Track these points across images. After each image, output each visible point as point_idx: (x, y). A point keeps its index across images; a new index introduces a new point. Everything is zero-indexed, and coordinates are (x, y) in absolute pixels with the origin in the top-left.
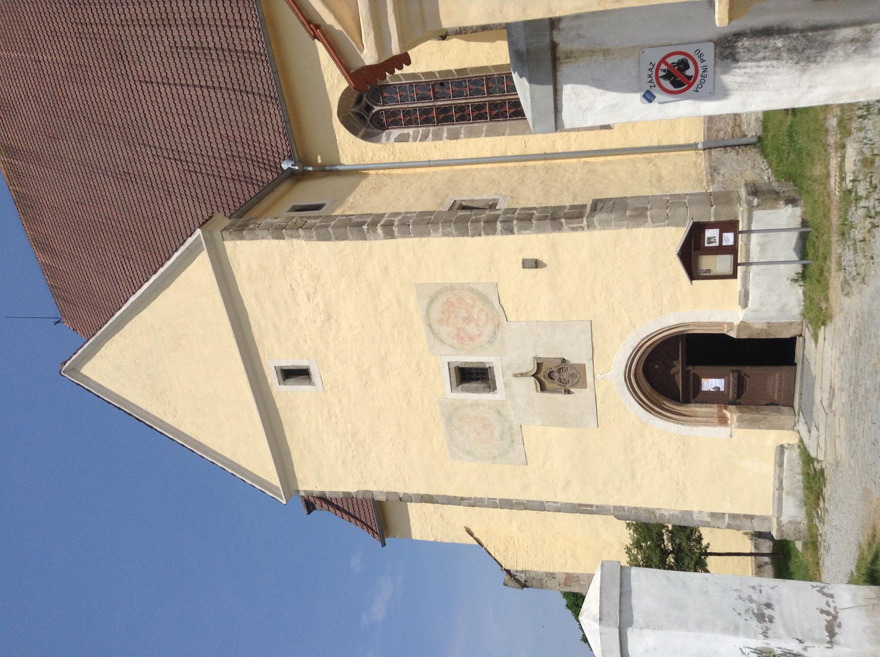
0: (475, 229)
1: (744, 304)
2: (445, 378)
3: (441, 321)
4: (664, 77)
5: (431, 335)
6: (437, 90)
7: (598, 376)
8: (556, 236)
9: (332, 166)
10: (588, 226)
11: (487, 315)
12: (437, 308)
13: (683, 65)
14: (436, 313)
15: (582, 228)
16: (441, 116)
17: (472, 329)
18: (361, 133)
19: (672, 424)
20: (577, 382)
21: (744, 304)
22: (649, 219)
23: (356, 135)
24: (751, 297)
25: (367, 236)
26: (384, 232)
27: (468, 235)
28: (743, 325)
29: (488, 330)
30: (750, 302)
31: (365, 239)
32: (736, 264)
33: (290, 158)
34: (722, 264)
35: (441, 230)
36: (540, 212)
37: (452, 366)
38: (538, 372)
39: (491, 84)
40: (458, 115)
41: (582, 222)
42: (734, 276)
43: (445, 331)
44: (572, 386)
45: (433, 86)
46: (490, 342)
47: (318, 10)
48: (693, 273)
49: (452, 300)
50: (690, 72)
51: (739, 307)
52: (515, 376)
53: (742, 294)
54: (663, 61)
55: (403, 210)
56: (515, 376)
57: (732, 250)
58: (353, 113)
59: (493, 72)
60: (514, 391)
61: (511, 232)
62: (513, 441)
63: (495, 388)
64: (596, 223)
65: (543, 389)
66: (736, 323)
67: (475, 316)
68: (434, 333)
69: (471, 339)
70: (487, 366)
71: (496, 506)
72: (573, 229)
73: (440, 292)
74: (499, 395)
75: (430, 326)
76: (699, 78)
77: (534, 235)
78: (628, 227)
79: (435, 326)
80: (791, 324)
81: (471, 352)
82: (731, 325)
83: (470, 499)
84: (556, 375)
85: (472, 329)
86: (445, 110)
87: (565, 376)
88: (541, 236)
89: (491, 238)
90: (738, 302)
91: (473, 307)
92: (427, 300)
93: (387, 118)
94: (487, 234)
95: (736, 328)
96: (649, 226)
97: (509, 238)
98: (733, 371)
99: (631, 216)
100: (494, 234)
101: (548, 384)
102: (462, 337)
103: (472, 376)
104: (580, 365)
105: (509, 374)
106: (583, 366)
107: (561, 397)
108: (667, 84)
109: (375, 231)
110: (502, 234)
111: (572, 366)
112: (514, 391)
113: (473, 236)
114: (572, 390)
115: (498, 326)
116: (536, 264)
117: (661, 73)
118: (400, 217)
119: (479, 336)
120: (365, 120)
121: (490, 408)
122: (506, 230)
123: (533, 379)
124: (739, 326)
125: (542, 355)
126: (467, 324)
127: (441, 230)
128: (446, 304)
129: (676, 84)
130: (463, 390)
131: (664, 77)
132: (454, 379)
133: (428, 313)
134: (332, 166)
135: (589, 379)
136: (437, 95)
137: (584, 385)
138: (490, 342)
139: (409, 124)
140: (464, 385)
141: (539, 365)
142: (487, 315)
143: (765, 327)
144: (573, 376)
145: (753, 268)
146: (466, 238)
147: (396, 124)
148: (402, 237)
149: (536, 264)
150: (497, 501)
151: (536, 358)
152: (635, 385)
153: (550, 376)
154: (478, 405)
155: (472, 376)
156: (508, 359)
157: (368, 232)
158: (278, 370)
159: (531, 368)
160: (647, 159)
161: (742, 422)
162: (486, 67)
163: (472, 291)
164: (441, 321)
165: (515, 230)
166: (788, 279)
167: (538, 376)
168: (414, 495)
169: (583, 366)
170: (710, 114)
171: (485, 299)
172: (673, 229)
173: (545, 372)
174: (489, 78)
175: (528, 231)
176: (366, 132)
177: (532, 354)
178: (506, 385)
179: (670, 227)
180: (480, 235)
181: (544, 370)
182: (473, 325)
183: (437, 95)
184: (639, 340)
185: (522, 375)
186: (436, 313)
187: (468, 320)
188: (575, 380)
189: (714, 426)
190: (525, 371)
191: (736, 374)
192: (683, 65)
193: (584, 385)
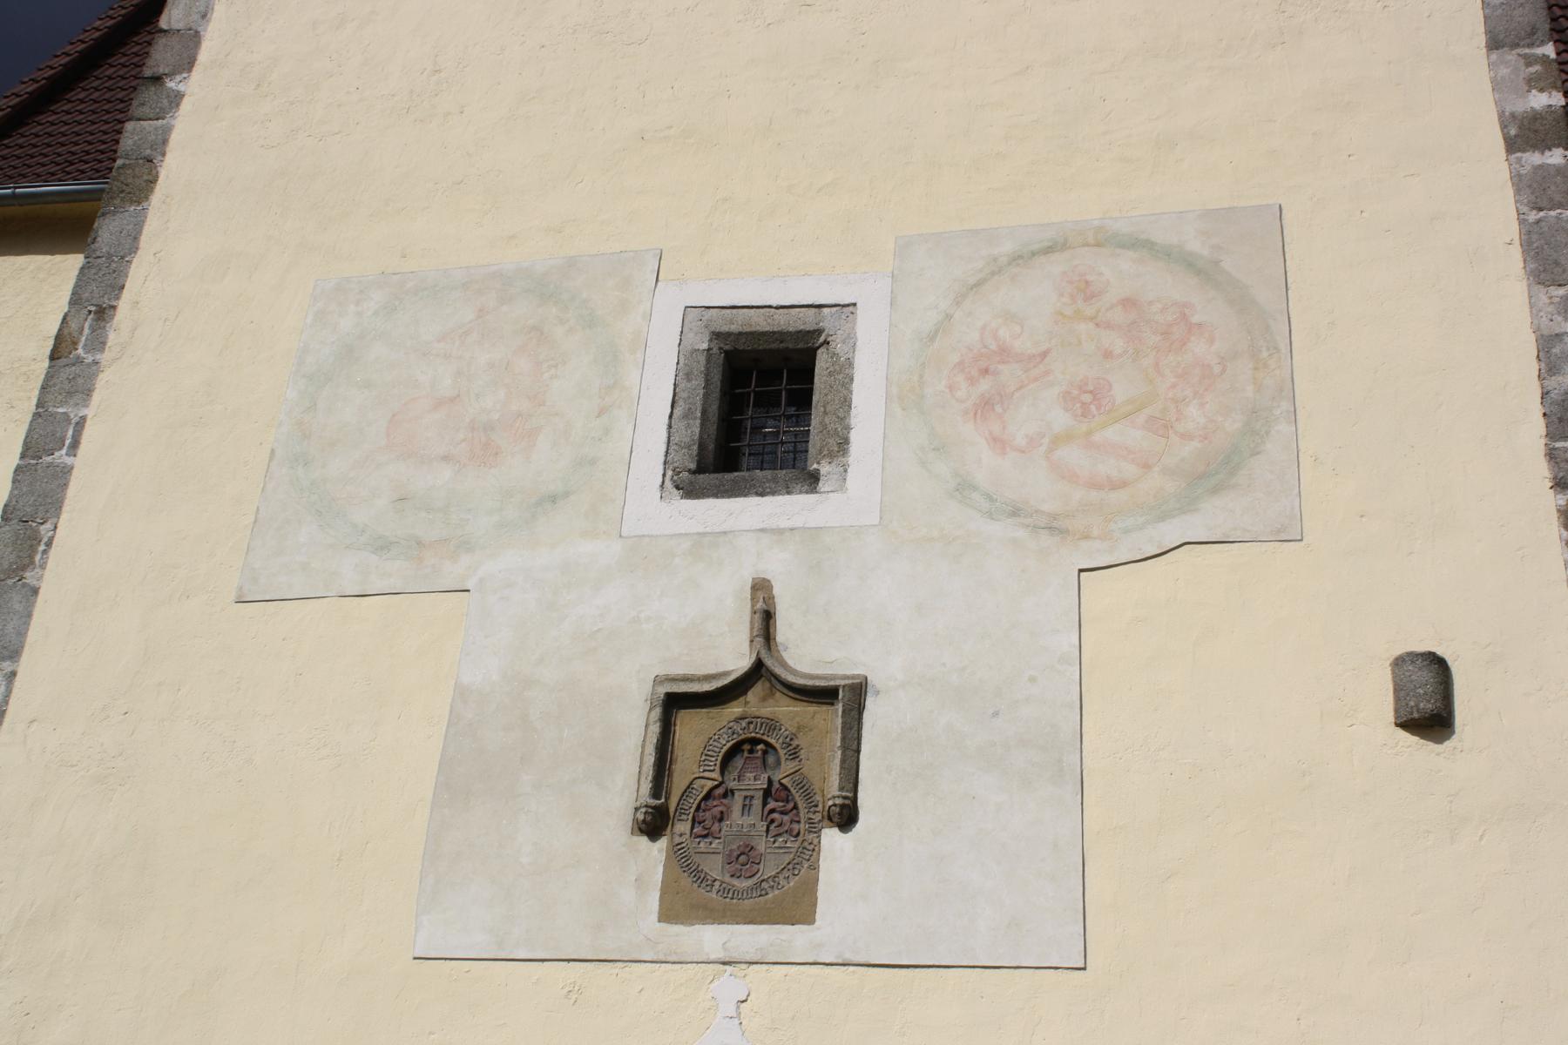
2: (765, 282)
3: (1086, 290)
5: (1007, 247)
7: (729, 985)
11: (1124, 484)
12: (1164, 287)
14: (1118, 274)
17: (1039, 412)
20: (700, 877)
25: (1511, 56)
26: (1535, 117)
27: (1551, 435)
37: (828, 320)
43: (1035, 300)
52: (761, 587)
62: (383, 546)
63: (690, 491)
71: (33, 449)
79: (1056, 265)
83: (98, 343)
84: (753, 781)
87: (743, 821)
92: (1195, 245)
104: (809, 891)
106: (800, 909)
109: (1533, 83)
115: (1054, 527)
116: (1428, 708)
133: (1140, 244)
135: (712, 938)
137: (678, 907)
138: (963, 488)
142: (1124, 484)
146: (1538, 426)
149: (1428, 708)
150: (61, 456)
156: (837, 566)
159: (807, 653)
160: (1525, 56)
168: (168, 130)
169: (800, 909)
170: (1481, 40)
178: (704, 543)
182: (1060, 419)
185: (767, 618)
186: (1118, 274)
187: (1088, 400)
188: (714, 867)
190: (784, 631)
193: (678, 907)
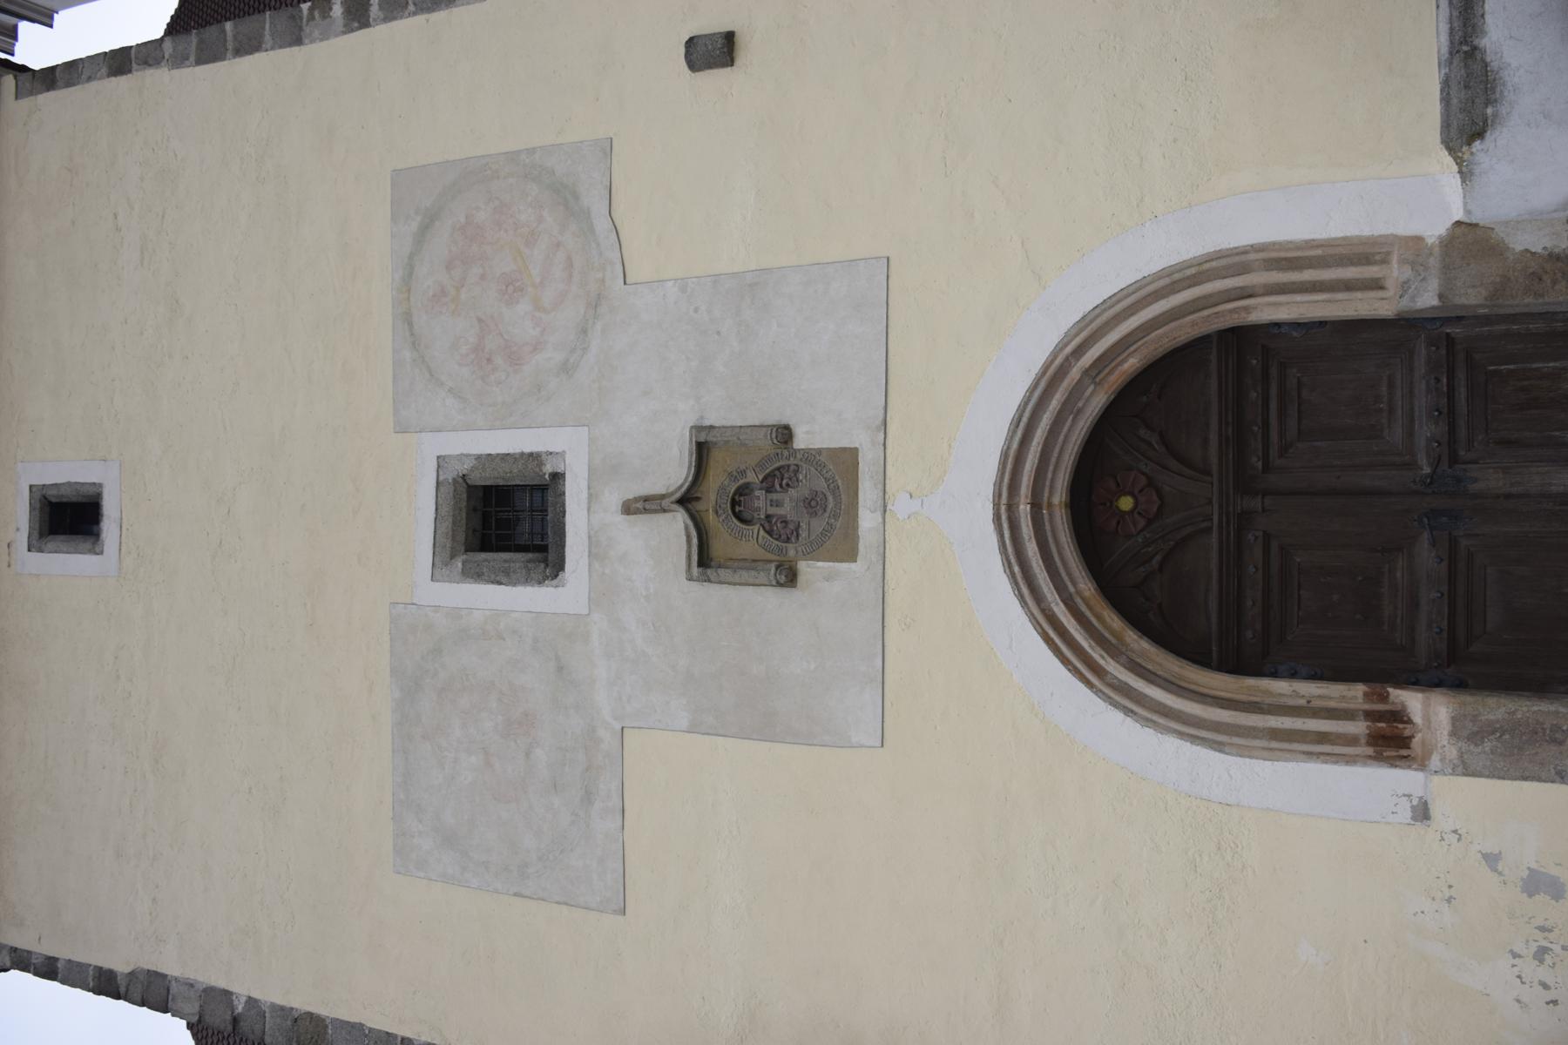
2: (418, 517)
19: (1171, 743)
28: (1469, 240)
37: (449, 475)
52: (629, 508)
60: (619, 553)
62: (588, 797)
63: (559, 566)
68: (415, 345)
74: (568, 595)
75: (407, 318)
84: (760, 502)
87: (787, 505)
101: (1458, 231)
105: (613, 498)
106: (848, 458)
107: (766, 600)
115: (596, 303)
119: (537, 347)
125: (720, 415)
141: (702, 451)
142: (569, 258)
144: (813, 504)
152: (1032, 549)
155: (505, 520)
156: (610, 449)
158: (37, 496)
159: (674, 473)
161: (1476, 737)
168: (273, 1006)
169: (848, 458)
178: (596, 551)
181: (717, 483)
182: (524, 307)
187: (512, 288)
188: (818, 525)
189: (1350, 760)
190: (659, 489)
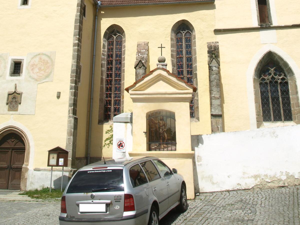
0: (73, 76)
1: (36, 170)
2: (18, 57)
3: (41, 59)
4: (121, 143)
5: (35, 54)
6: (119, 61)
7: (12, 116)
8: (67, 105)
9: (97, 19)
10: (70, 116)
11: (41, 77)
13: (122, 146)
14: (44, 57)
15: (69, 114)
16: (110, 61)
17: (36, 70)
18: (107, 31)
21: (36, 170)
22: (70, 137)
23: (107, 30)
24: (38, 172)
25: (75, 37)
27: (71, 73)
28: (27, 170)
29: (35, 76)
30: (36, 172)
31: (74, 36)
32: (52, 166)
33: (101, 4)
34: (53, 161)
35: (74, 64)
36: (76, 99)
37: (22, 61)
38: (16, 93)
39: (118, 81)
40: (109, 68)
41: (71, 114)
42: (49, 165)
43: (37, 59)
44: (9, 106)
45: (120, 60)
46: (30, 77)
47: (142, 82)
48: (51, 152)
49: (48, 64)
50: (121, 147)
51: (34, 168)
52: (16, 85)
53: (39, 169)
54: (123, 142)
55: (81, 50)
56: (16, 85)
57: (57, 165)
58: (115, 29)
59: (122, 82)
60: (9, 83)
61: (71, 89)
63: (11, 76)
64: (70, 119)
65: (9, 94)
66: (28, 167)
67: (41, 72)
68: (36, 55)
69: (32, 69)
70: (21, 74)
72: (69, 111)
73: (52, 60)
75: (39, 54)
76: (120, 149)
77: (69, 97)
78: (67, 130)
79: (39, 56)
80: (26, 186)
81: (27, 68)
82: (28, 165)
84: (14, 100)
85: (36, 70)
86: (112, 63)
87: (14, 103)
88: (68, 99)
89: (70, 81)
90: (36, 167)
91: (45, 72)
92: (49, 55)
93: (111, 41)
94: (71, 80)
95: (26, 167)
96: (67, 137)
97: (69, 88)
98: (8, 166)
99: (71, 131)
100: (71, 83)
101: (11, 96)
102: (33, 66)
103: (17, 68)
105: (17, 83)
106: (17, 110)
108: (119, 143)
109: (76, 40)
110: (70, 85)
111: (18, 106)
112: (9, 83)
113: (71, 75)
114: (8, 105)
115: (36, 80)
116: (58, 97)
117: (121, 142)
118: (80, 49)
119: (33, 73)
120: (111, 33)
121: (3, 73)
122: (72, 87)
123: (14, 91)
124: (27, 168)
125: (23, 95)
126: (38, 69)
127: (74, 64)
128: (47, 63)
129: (119, 145)
130: (11, 63)
131: (121, 143)
132: (17, 61)
134: (97, 19)
135: (11, 112)
136: (117, 61)
137: (9, 110)
138: (30, 77)
139: (109, 49)
140: (14, 63)
143: (25, 177)
145: (50, 173)
147: (109, 45)
148: (73, 49)
149: (58, 97)
151: (22, 93)
153: (14, 98)
154: (5, 68)
155: (17, 68)
156: (22, 82)
157: (76, 38)
159: (19, 91)
162: (124, 80)
163: (51, 72)
164: (41, 59)
165: (71, 90)
166: (43, 185)
167: (15, 93)
169: (17, 110)
171: (47, 76)
172: (65, 145)
173: (16, 96)
174: (120, 80)
175: (70, 95)
176: (107, 33)
177: (24, 92)
178: (12, 81)
179: (66, 144)
180: (71, 78)
182: (38, 71)
183: (117, 61)
184: (25, 132)
185: (16, 87)
187: (40, 69)
190: (17, 88)
191: (7, 167)
192: (122, 146)
193: (9, 110)
